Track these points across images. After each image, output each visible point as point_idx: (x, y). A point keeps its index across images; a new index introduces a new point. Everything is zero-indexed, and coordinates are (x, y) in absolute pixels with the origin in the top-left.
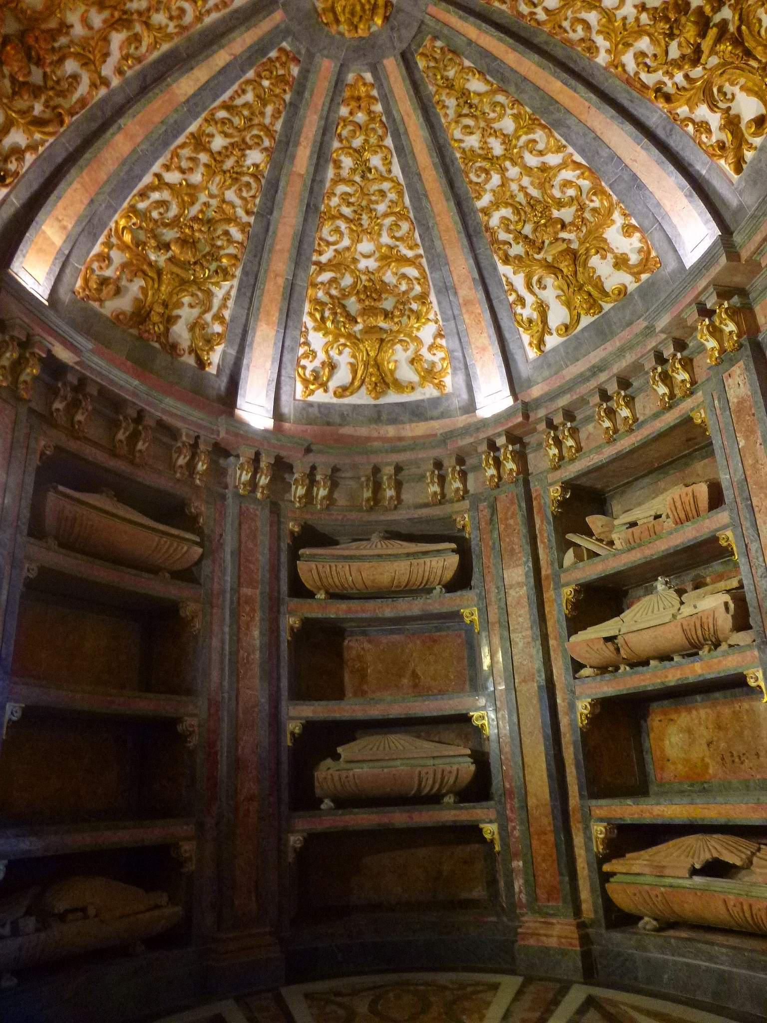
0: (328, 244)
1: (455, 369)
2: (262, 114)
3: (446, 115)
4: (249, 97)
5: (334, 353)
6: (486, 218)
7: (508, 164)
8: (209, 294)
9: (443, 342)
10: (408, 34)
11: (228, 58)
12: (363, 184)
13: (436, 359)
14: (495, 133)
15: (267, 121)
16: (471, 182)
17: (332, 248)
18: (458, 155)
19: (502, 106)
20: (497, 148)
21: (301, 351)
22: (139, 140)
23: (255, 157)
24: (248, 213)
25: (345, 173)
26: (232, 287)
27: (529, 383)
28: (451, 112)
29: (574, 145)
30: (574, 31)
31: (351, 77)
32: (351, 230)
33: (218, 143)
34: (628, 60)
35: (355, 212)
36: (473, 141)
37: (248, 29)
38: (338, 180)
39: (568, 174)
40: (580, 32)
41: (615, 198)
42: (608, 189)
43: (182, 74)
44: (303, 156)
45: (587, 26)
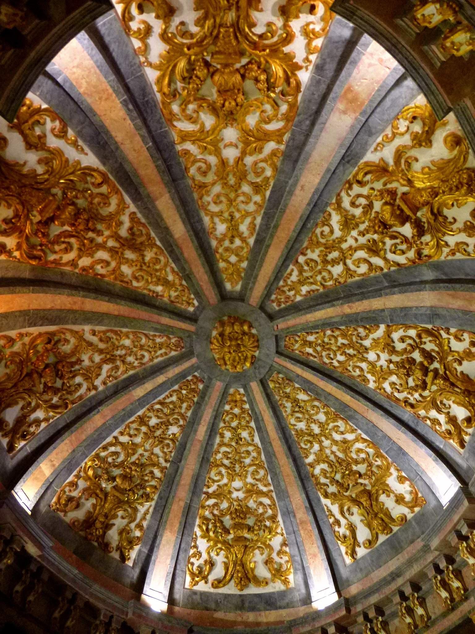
0: (214, 481)
1: (296, 570)
2: (181, 407)
3: (286, 411)
4: (174, 398)
5: (213, 554)
6: (312, 469)
7: (323, 438)
8: (136, 510)
9: (287, 549)
10: (264, 371)
11: (164, 379)
12: (236, 447)
13: (283, 561)
14: (315, 421)
15: (183, 411)
16: (301, 448)
17: (216, 484)
18: (293, 433)
19: (318, 407)
20: (316, 430)
21: (192, 552)
22: (108, 418)
23: (174, 430)
24: (166, 461)
25: (226, 440)
26: (150, 506)
27: (348, 583)
28: (289, 410)
29: (361, 429)
30: (355, 371)
31: (232, 391)
32: (228, 473)
33: (153, 421)
34: (386, 386)
35: (231, 463)
36: (302, 425)
37: (177, 366)
38: (222, 444)
39: (359, 445)
40: (358, 372)
41: (390, 460)
42: (384, 454)
43: (139, 386)
44: (202, 431)
45: (362, 370)
